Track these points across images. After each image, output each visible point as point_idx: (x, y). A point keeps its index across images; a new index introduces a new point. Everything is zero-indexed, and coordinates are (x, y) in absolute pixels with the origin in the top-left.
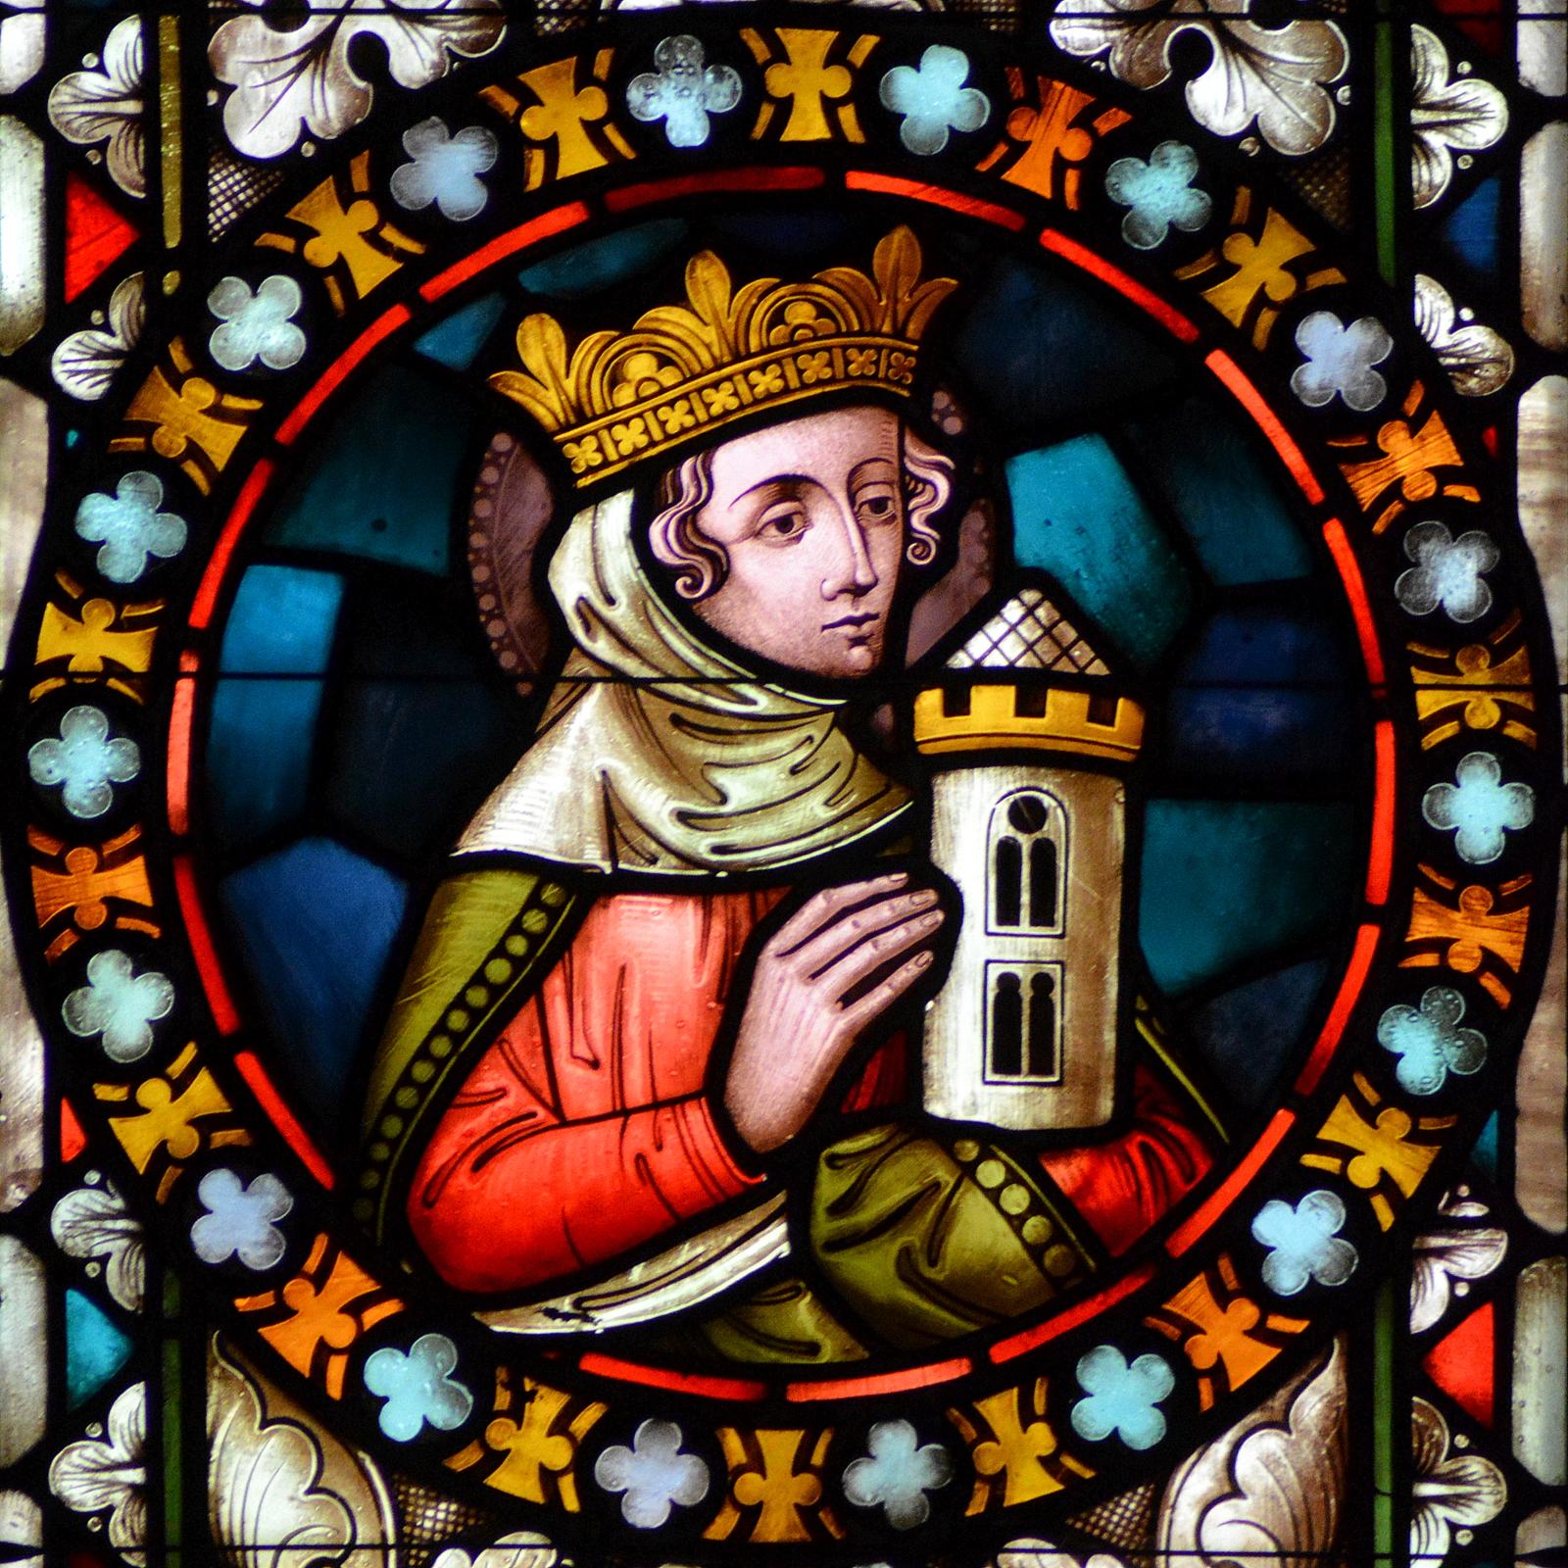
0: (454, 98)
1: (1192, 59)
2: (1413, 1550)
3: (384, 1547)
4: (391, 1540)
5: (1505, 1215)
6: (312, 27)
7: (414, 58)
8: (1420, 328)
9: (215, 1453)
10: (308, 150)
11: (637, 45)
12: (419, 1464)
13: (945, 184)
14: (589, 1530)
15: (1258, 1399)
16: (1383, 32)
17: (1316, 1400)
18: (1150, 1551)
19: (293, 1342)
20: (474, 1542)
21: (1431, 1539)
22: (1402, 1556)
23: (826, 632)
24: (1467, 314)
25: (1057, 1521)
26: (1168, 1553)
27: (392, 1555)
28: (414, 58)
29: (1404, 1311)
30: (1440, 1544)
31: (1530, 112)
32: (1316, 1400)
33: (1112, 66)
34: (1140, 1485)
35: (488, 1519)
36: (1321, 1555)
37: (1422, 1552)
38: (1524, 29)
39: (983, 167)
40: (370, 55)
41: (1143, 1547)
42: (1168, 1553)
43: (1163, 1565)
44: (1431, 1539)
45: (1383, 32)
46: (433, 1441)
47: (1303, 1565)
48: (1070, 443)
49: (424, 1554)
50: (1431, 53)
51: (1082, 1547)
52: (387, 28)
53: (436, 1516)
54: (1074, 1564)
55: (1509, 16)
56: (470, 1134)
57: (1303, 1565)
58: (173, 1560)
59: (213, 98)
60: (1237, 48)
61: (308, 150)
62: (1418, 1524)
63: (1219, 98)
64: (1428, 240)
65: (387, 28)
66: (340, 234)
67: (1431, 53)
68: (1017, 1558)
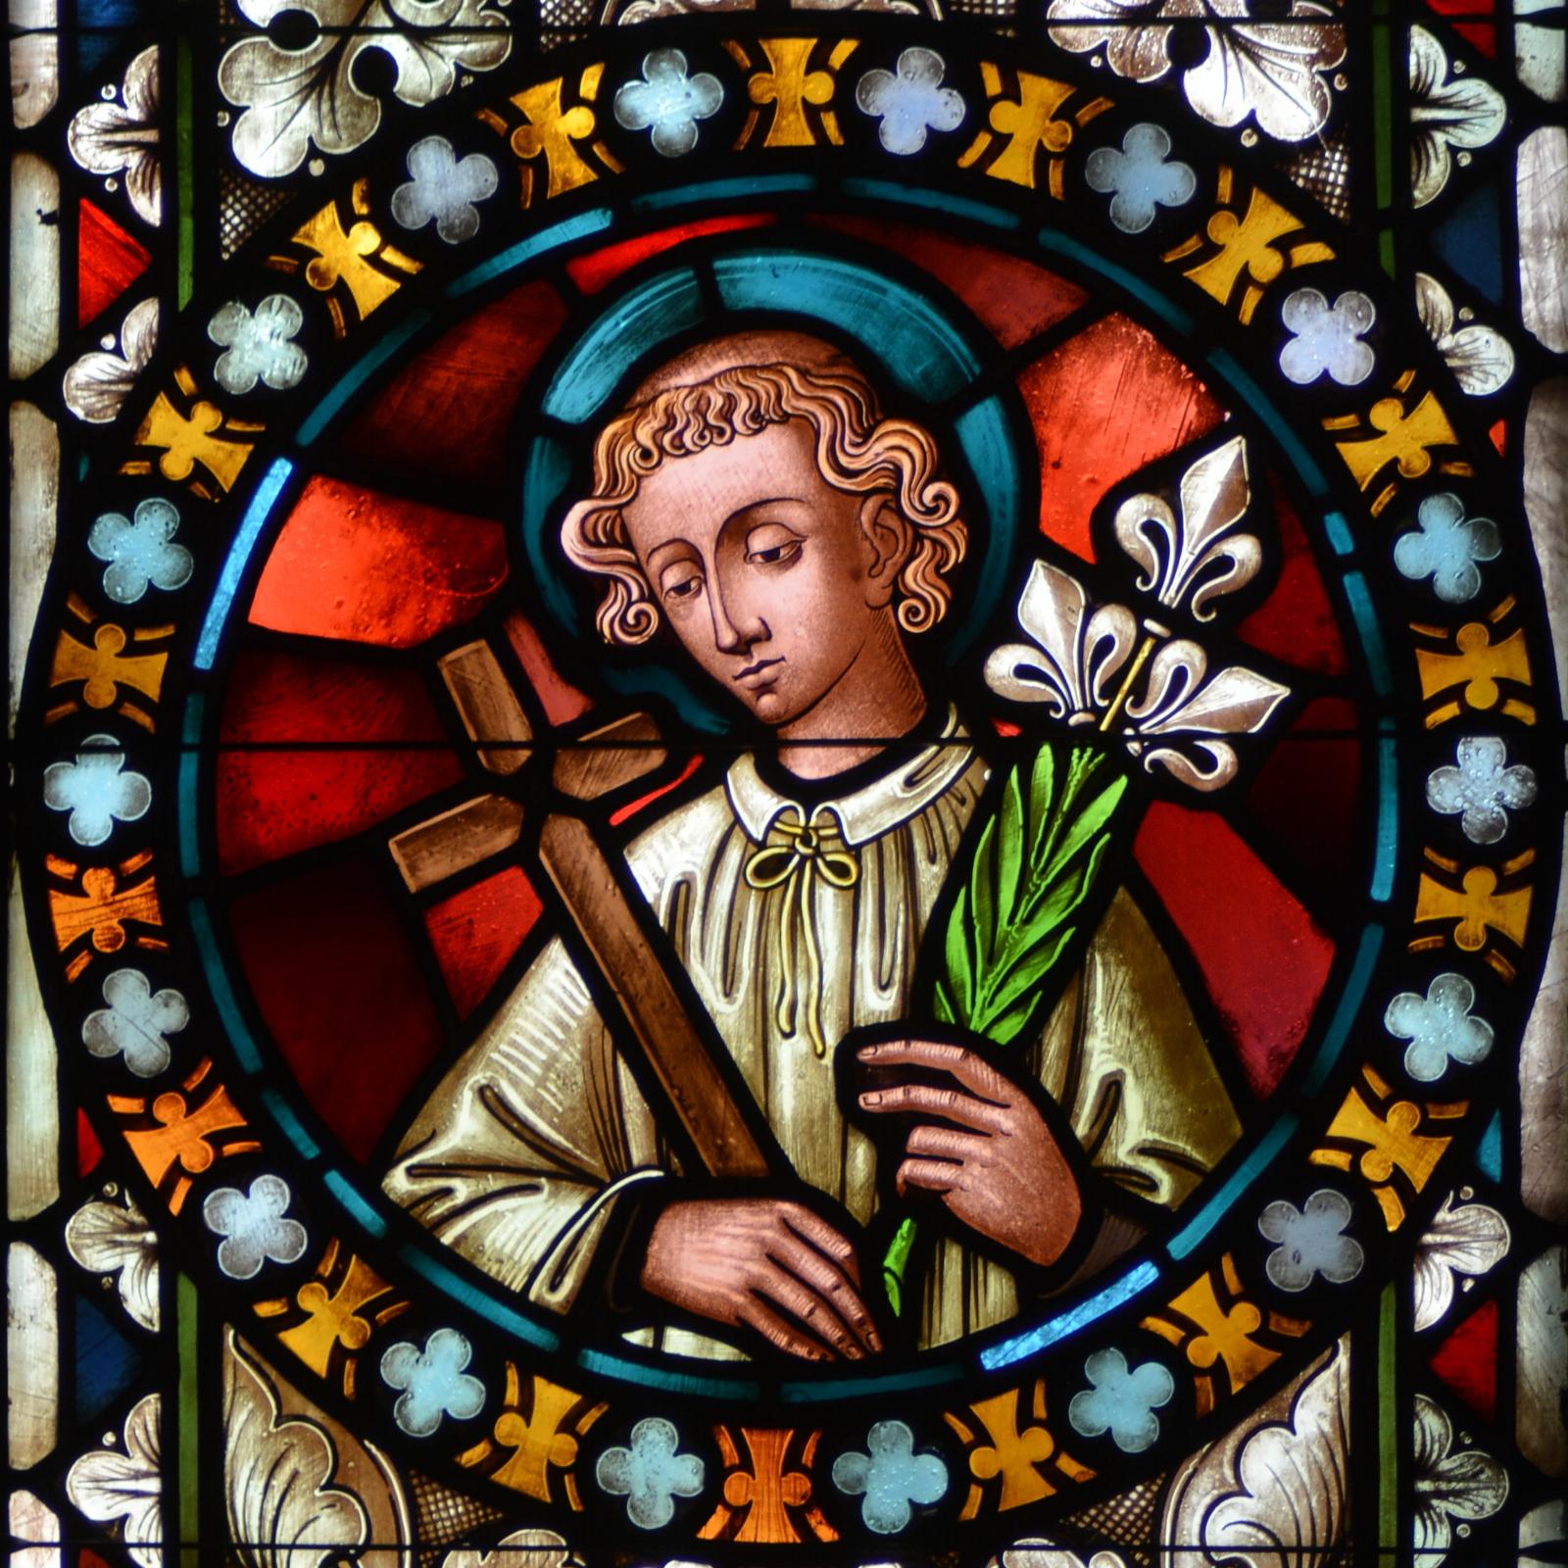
0: (471, 115)
1: (1188, 49)
2: (1418, 1542)
3: (400, 1548)
4: (408, 1541)
5: (1502, 1195)
6: (321, 44)
7: (420, 75)
8: (1425, 325)
9: (231, 1445)
10: (317, 168)
11: (627, 53)
12: (432, 1457)
13: (929, 185)
14: (593, 1521)
15: (1264, 1397)
16: (1381, 36)
17: (1319, 1403)
18: (1154, 1548)
19: (310, 1344)
20: (482, 1539)
21: (1431, 1537)
22: (1406, 1552)
23: (429, 1132)
24: (109, 342)
25: (1060, 1520)
26: (1174, 1548)
27: (407, 1555)
28: (420, 75)
29: (1406, 1307)
30: (1442, 1538)
31: (1528, 112)
32: (1319, 1403)
33: (1111, 61)
34: (1141, 1483)
35: (499, 1515)
36: (1324, 1550)
37: (1428, 1546)
38: (1525, 33)
39: (1429, 853)
40: (378, 71)
41: (1146, 1549)
42: (1174, 1548)
43: (1167, 1564)
44: (1431, 1537)
45: (1381, 36)
46: (453, 1432)
47: (1306, 1564)
48: (1013, 1292)
49: (437, 1553)
50: (1425, 51)
51: (1084, 1546)
52: (396, 46)
53: (449, 1511)
54: (1079, 1564)
55: (1504, 19)
56: (895, 564)
57: (1306, 1564)
58: (189, 1559)
59: (224, 118)
60: (1238, 44)
61: (317, 168)
62: (1429, 1269)
63: (1217, 90)
64: (1426, 237)
65: (396, 46)
66: (348, 250)
67: (1425, 51)
68: (1020, 1555)
